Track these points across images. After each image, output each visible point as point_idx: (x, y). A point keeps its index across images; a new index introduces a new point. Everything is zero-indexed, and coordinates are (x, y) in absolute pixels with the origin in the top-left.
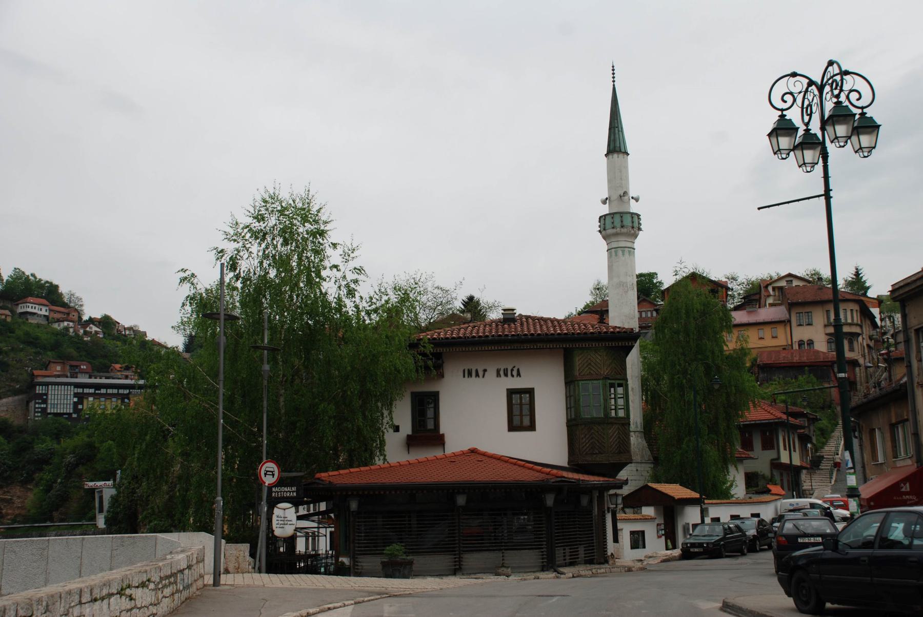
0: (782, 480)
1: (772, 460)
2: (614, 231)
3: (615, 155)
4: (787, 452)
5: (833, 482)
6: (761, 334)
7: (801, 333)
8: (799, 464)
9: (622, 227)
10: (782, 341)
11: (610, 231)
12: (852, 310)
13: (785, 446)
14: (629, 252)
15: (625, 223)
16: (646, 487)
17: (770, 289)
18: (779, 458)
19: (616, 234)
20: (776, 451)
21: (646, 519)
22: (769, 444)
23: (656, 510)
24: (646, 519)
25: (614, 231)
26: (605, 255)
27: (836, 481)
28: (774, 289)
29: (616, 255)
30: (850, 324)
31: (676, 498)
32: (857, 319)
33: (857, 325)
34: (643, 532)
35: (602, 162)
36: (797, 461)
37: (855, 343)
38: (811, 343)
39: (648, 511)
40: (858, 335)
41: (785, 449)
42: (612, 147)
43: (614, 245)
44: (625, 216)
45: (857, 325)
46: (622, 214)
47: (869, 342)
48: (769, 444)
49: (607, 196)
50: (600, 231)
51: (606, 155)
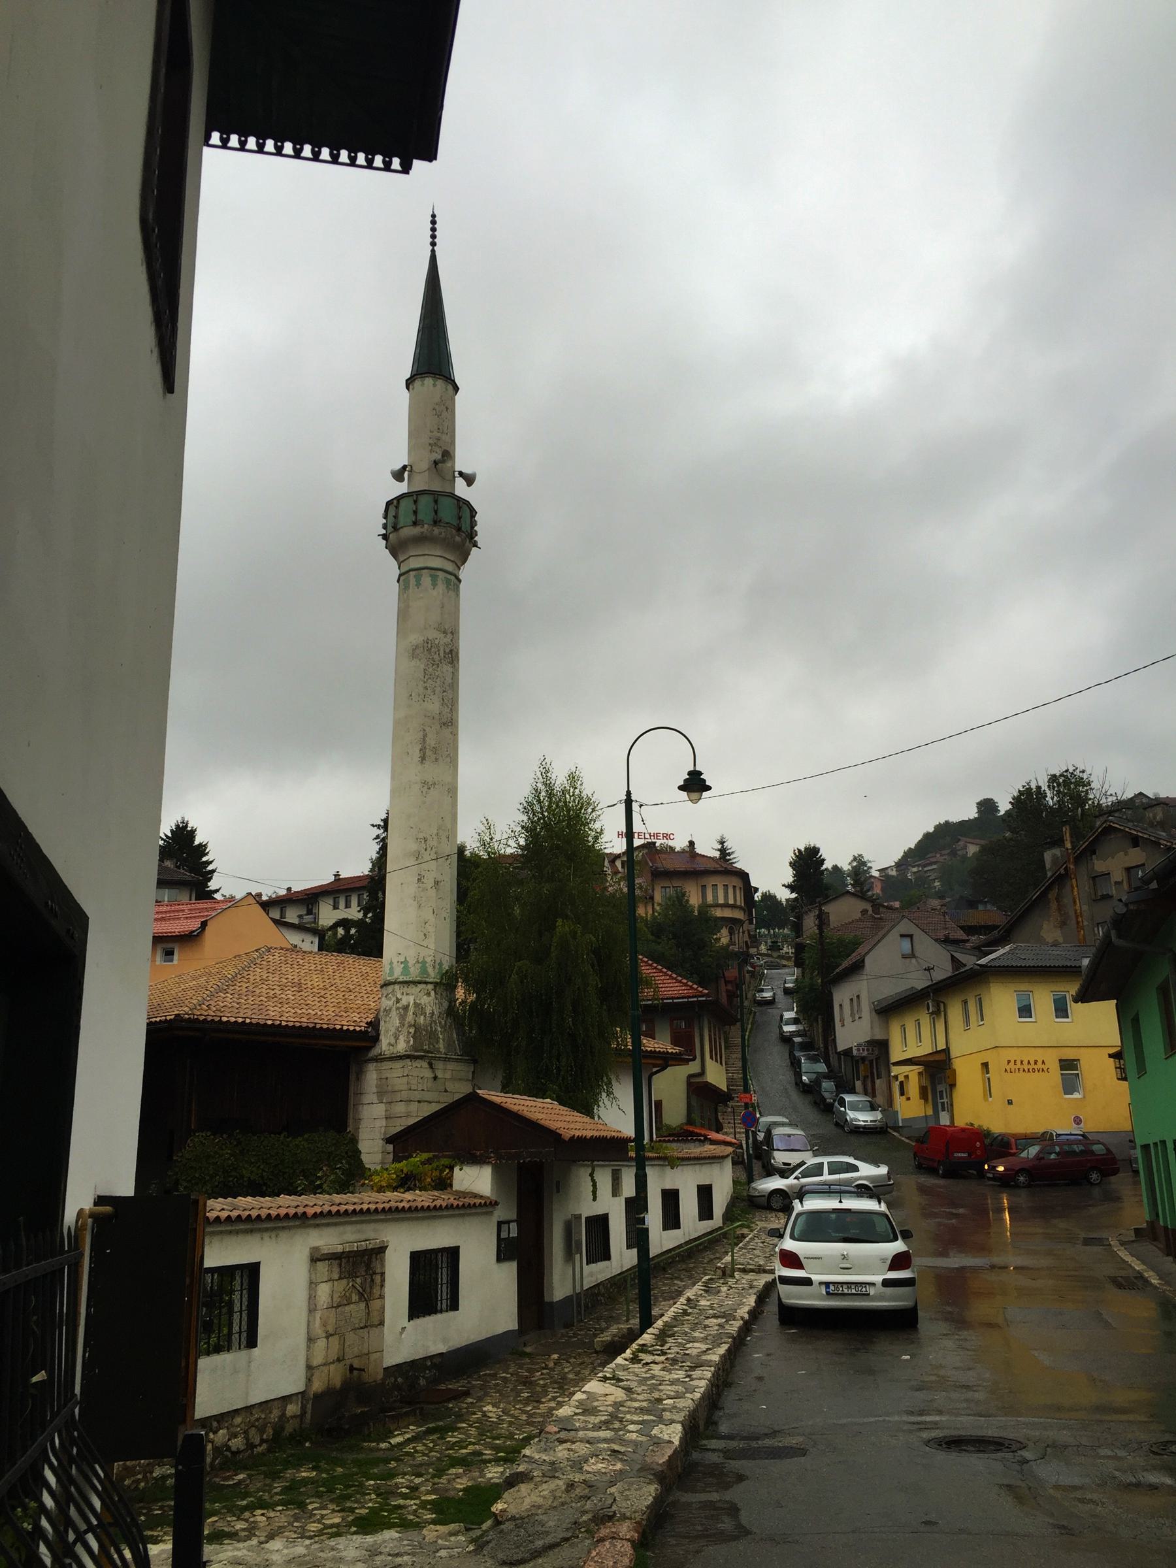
1: (690, 1076)
2: (416, 531)
11: (408, 532)
12: (734, 887)
14: (448, 582)
15: (441, 514)
16: (472, 1098)
18: (703, 1073)
19: (419, 540)
21: (470, 1207)
24: (470, 1207)
25: (416, 531)
26: (393, 588)
29: (418, 585)
30: (726, 905)
31: (567, 1135)
32: (740, 901)
33: (740, 908)
34: (453, 1253)
35: (399, 402)
39: (476, 1180)
41: (711, 1058)
43: (415, 563)
46: (436, 496)
50: (385, 537)
51: (409, 383)
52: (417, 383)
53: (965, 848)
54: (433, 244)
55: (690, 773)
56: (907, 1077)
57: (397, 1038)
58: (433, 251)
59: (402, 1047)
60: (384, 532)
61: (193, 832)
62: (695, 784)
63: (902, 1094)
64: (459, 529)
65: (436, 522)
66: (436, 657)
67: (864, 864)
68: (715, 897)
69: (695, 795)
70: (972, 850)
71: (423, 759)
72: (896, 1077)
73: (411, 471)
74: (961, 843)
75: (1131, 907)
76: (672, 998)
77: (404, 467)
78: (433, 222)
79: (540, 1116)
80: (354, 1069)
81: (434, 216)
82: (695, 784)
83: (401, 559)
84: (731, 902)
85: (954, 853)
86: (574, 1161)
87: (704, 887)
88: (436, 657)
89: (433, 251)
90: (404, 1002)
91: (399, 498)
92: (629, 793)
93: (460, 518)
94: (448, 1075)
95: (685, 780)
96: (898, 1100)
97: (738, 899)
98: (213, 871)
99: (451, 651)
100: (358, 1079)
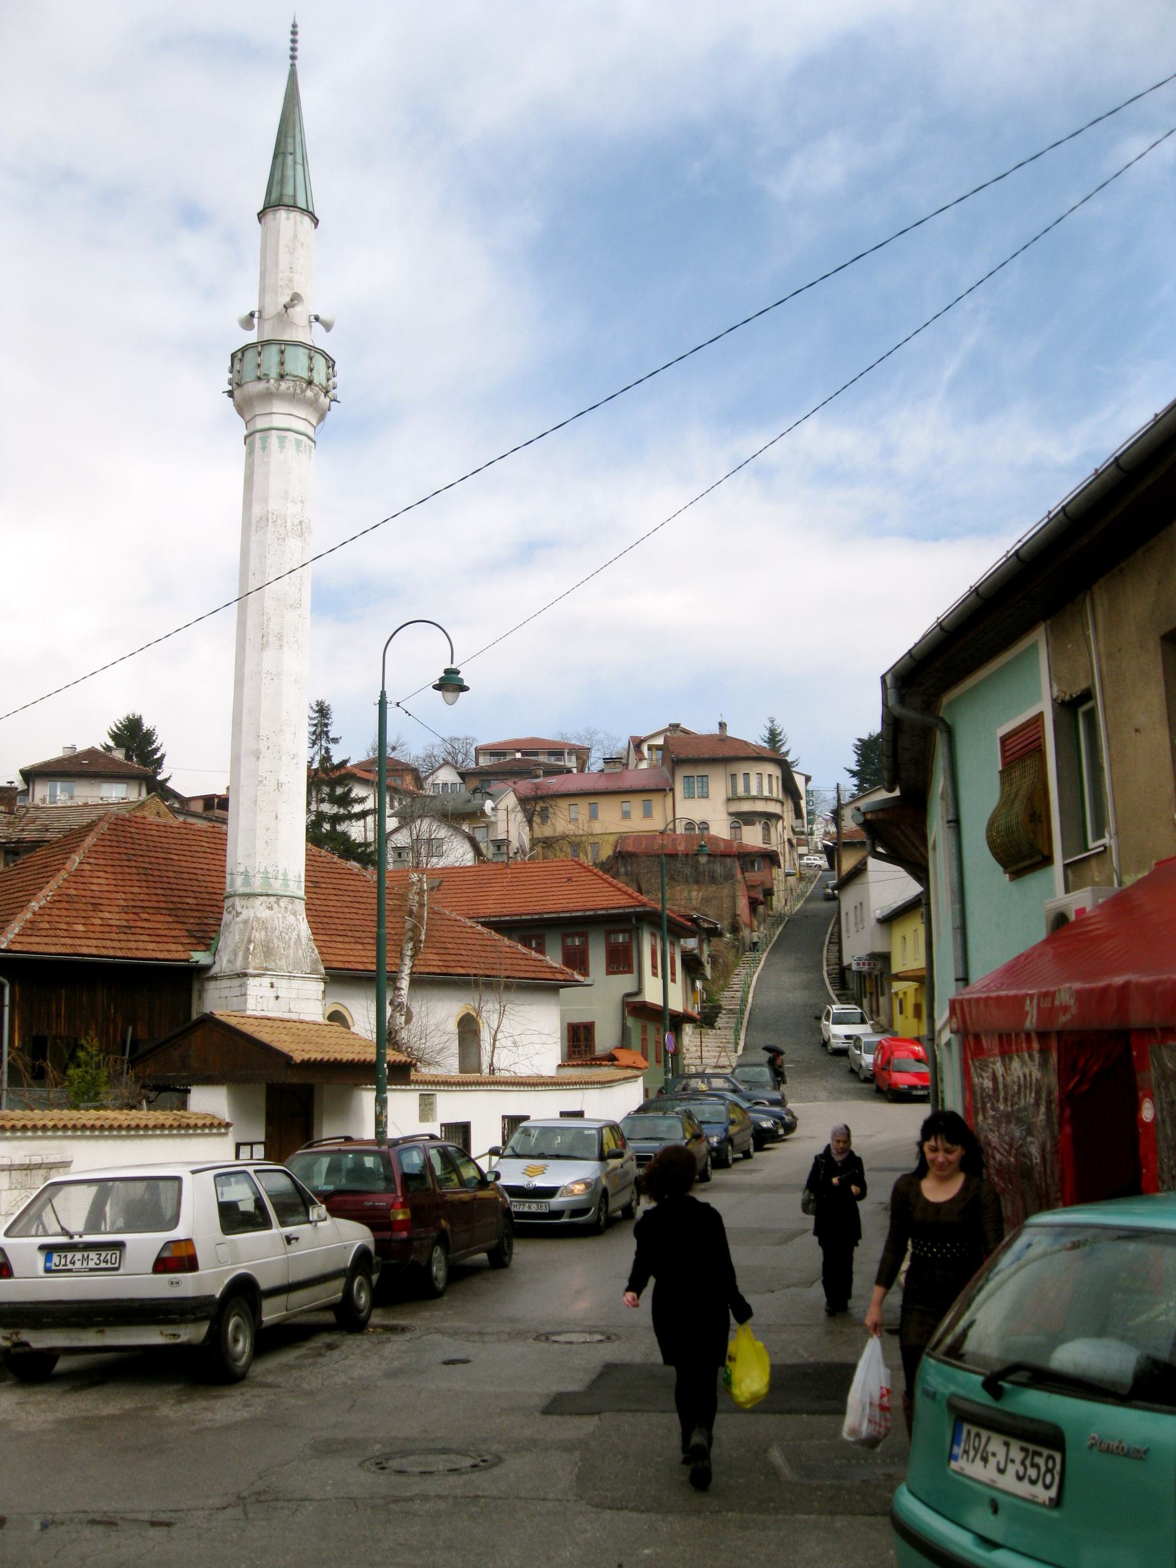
0: (644, 1040)
3: (282, 214)
4: (660, 981)
5: (740, 1052)
6: (626, 806)
7: (690, 809)
8: (680, 1010)
9: (282, 377)
10: (656, 823)
13: (654, 966)
15: (289, 367)
17: (645, 748)
18: (639, 992)
20: (635, 975)
22: (621, 960)
23: (238, 1103)
25: (261, 386)
27: (745, 1049)
28: (650, 748)
29: (264, 448)
30: (767, 799)
31: (298, 1057)
32: (777, 792)
33: (777, 801)
36: (677, 1003)
37: (773, 830)
38: (704, 826)
39: (208, 1101)
40: (778, 817)
41: (655, 974)
42: (274, 196)
44: (290, 351)
45: (777, 801)
47: (791, 835)
48: (621, 960)
49: (255, 308)
50: (231, 394)
52: (269, 217)
54: (293, 58)
55: (447, 671)
56: (905, 993)
58: (293, 65)
60: (230, 388)
62: (451, 683)
63: (901, 1012)
64: (310, 383)
66: (282, 530)
68: (747, 788)
69: (450, 695)
72: (896, 994)
73: (260, 318)
75: (869, 817)
76: (596, 910)
77: (252, 315)
78: (294, 33)
79: (273, 1038)
80: (196, 986)
81: (294, 26)
82: (451, 683)
83: (248, 418)
84: (766, 793)
86: (356, 1085)
87: (733, 776)
88: (282, 530)
89: (293, 65)
91: (244, 350)
92: (383, 694)
93: (311, 370)
94: (293, 994)
95: (441, 679)
96: (898, 1020)
97: (775, 790)
98: (163, 756)
99: (301, 523)
100: (200, 997)
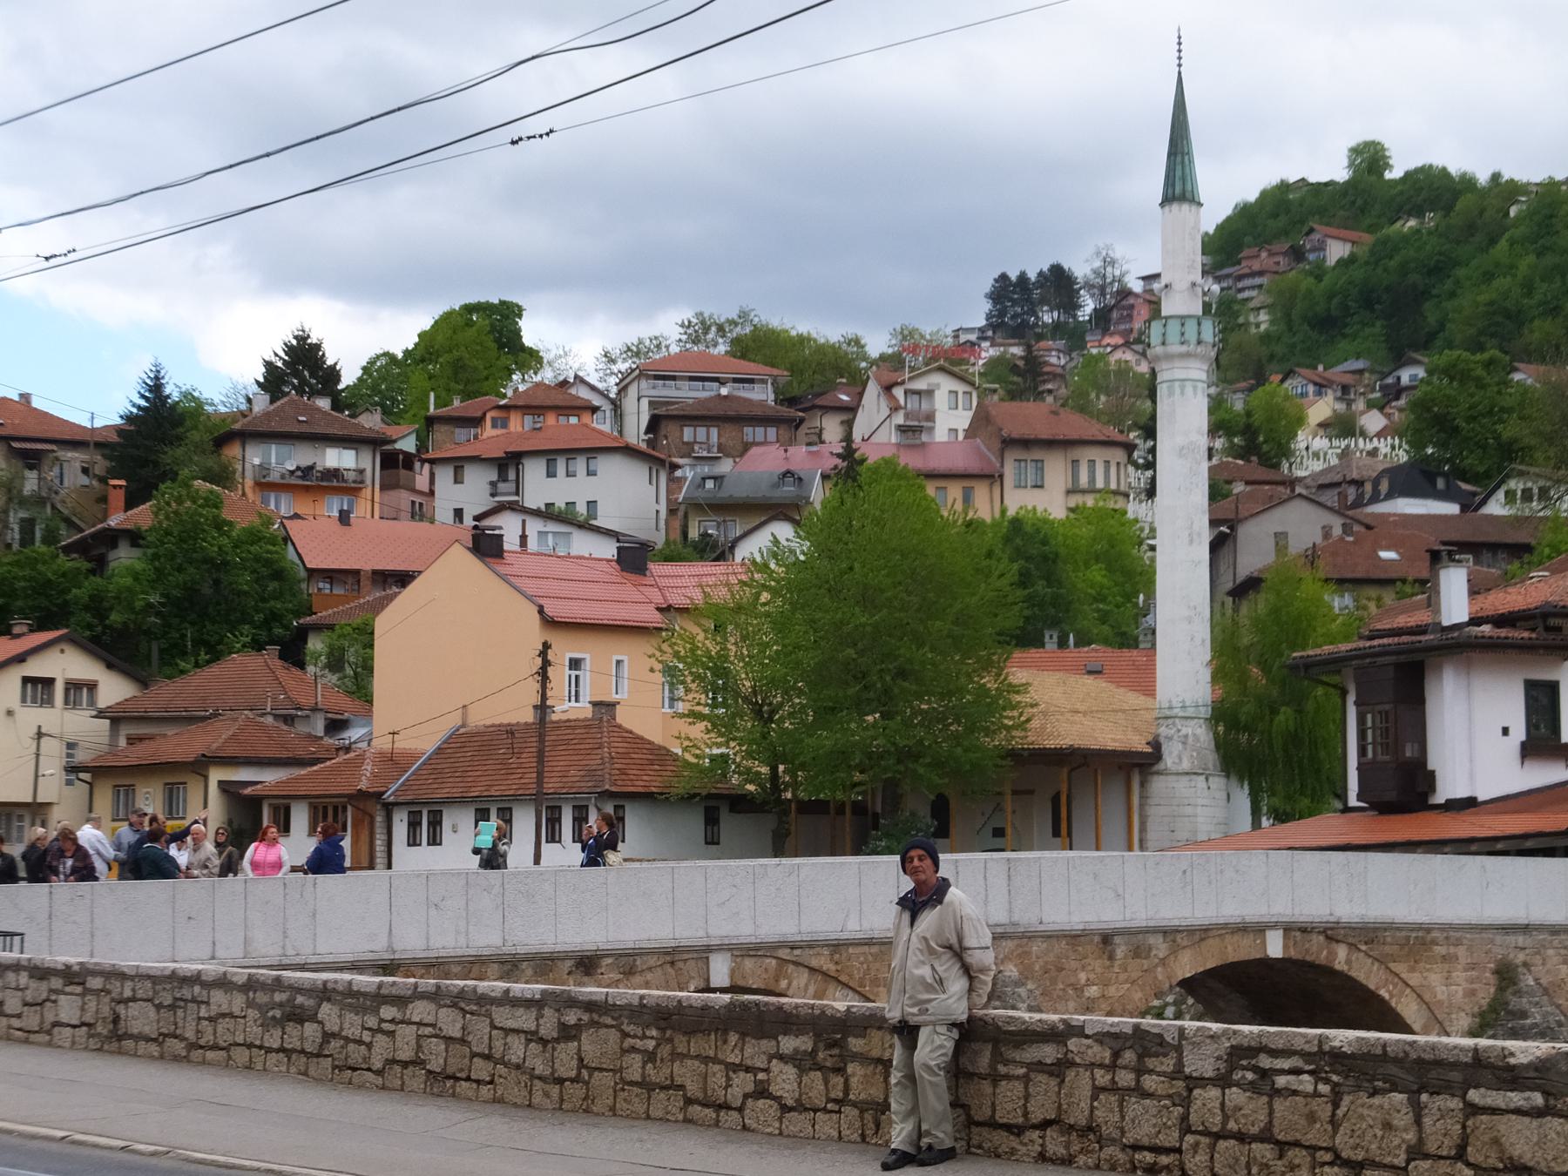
2: (1184, 349)
25: (1184, 349)
29: (1182, 393)
53: (1321, 247)
57: (1180, 759)
59: (1186, 765)
61: (318, 347)
65: (1199, 342)
67: (1113, 263)
68: (1092, 479)
70: (1336, 251)
71: (1191, 542)
74: (1316, 236)
84: (1100, 484)
85: (1297, 254)
87: (1075, 462)
90: (1184, 731)
